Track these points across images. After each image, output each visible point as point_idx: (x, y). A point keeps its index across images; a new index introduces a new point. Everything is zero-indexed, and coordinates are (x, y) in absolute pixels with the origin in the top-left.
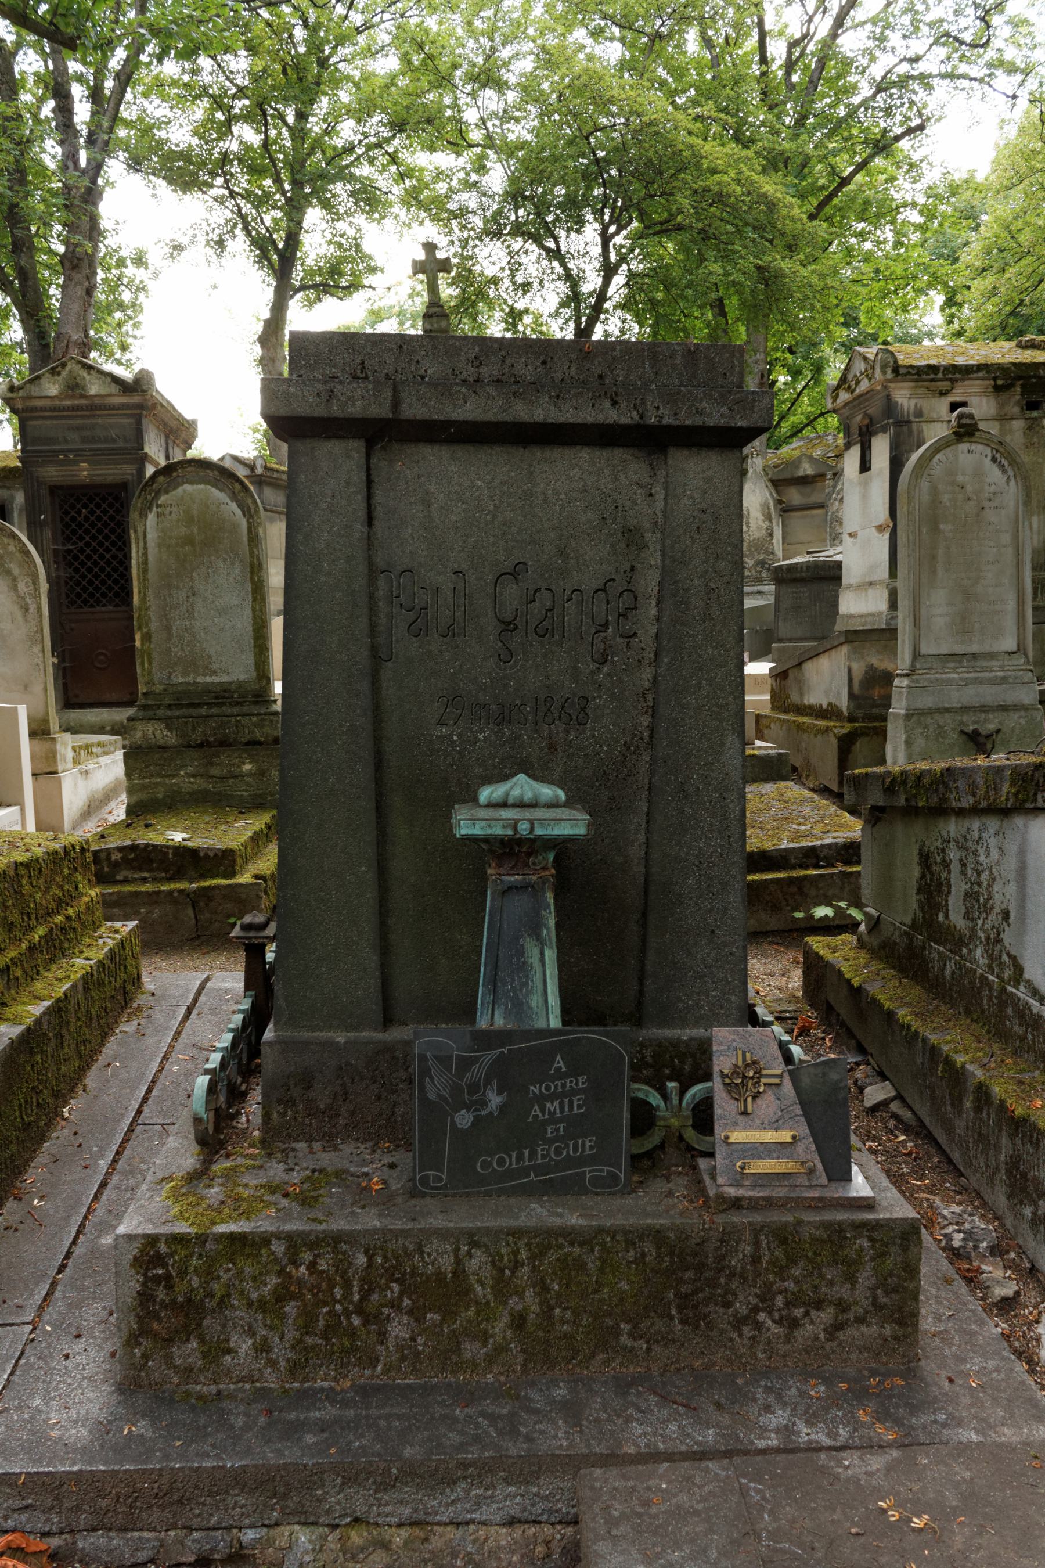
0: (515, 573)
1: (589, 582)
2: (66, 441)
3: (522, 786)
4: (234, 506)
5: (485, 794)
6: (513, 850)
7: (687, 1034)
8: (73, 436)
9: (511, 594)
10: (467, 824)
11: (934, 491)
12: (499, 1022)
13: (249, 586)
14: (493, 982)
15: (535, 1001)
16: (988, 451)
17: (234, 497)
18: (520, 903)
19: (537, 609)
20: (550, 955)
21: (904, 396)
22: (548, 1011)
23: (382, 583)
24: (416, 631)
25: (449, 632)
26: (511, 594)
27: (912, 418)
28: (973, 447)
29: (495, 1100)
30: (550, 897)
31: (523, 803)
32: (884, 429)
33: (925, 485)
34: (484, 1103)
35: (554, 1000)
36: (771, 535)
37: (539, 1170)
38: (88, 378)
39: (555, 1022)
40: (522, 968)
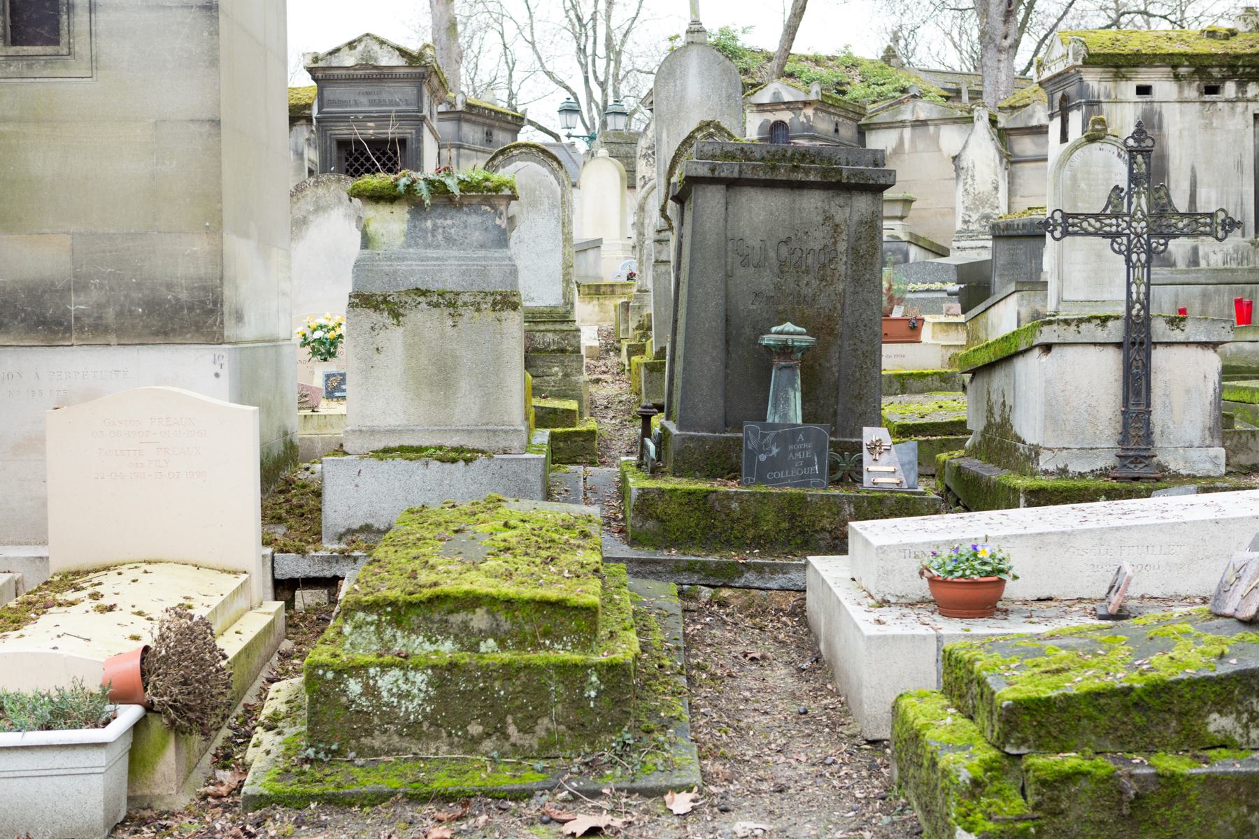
0: (787, 241)
1: (817, 247)
2: (356, 104)
3: (789, 327)
4: (552, 177)
5: (774, 329)
6: (785, 350)
7: (854, 440)
8: (364, 100)
9: (784, 251)
10: (767, 340)
11: (1074, 178)
12: (777, 421)
13: (560, 237)
14: (775, 406)
15: (791, 413)
16: (1115, 149)
17: (553, 171)
18: (786, 373)
19: (795, 258)
20: (798, 395)
21: (1095, 81)
22: (796, 414)
23: (730, 244)
24: (744, 264)
25: (757, 266)
26: (784, 251)
27: (1102, 99)
28: (1104, 146)
29: (775, 451)
30: (799, 372)
31: (789, 331)
32: (1078, 106)
33: (1066, 173)
34: (771, 451)
35: (799, 413)
36: (996, 189)
37: (793, 479)
38: (379, 51)
39: (799, 421)
40: (787, 400)
